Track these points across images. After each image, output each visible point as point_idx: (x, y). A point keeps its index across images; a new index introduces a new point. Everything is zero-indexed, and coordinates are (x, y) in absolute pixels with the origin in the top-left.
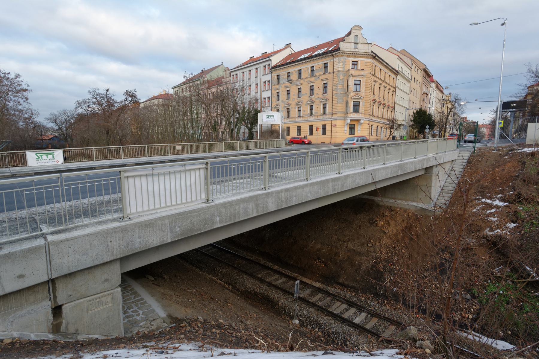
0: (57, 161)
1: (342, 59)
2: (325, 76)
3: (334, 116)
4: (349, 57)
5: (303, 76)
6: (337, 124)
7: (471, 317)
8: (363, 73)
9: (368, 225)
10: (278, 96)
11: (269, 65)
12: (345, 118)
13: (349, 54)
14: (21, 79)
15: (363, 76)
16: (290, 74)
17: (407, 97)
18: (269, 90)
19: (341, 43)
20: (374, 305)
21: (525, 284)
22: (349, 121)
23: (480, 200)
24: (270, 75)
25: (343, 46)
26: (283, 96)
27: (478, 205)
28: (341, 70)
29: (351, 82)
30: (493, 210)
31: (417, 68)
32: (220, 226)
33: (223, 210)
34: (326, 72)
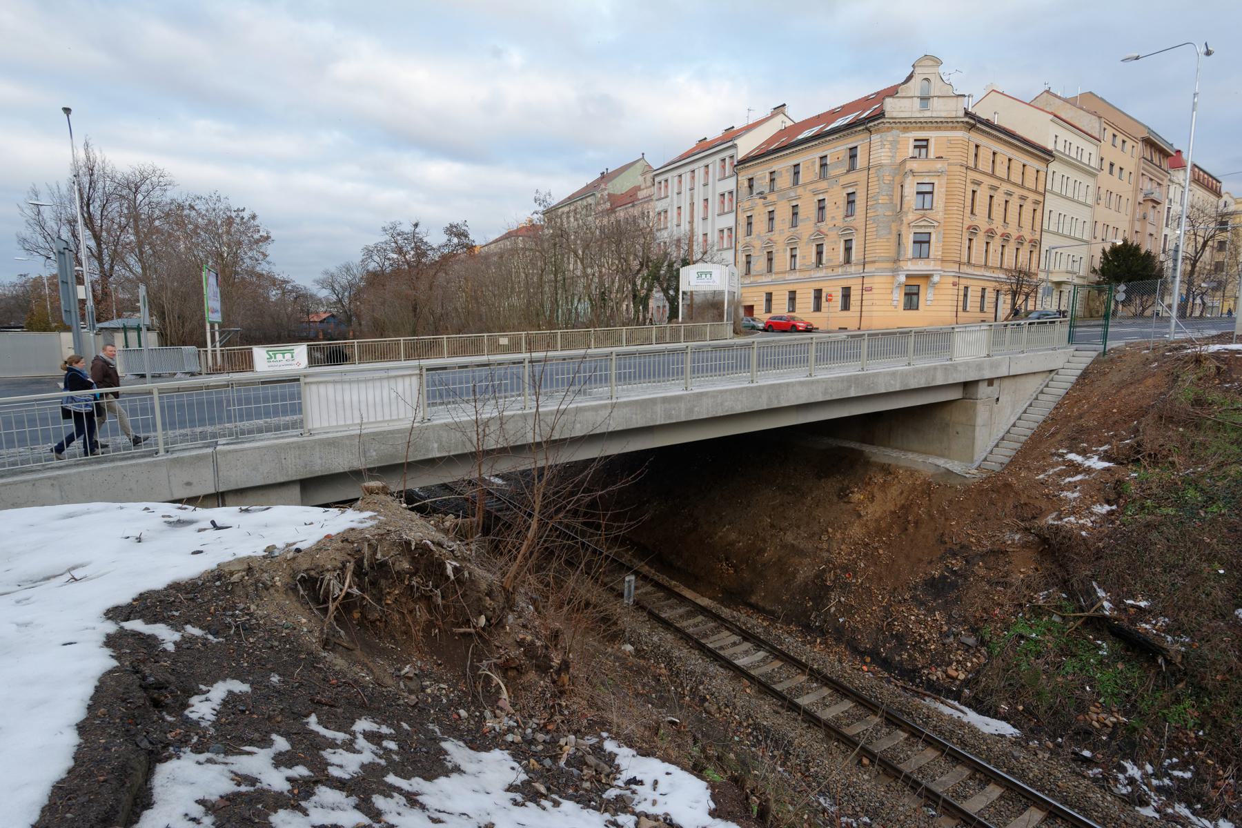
0: (298, 364)
2: (852, 177)
3: (868, 268)
4: (906, 130)
5: (802, 178)
6: (874, 286)
7: (962, 676)
8: (939, 165)
9: (835, 499)
10: (750, 224)
11: (732, 157)
13: (906, 124)
14: (256, 222)
15: (939, 174)
17: (1084, 214)
18: (731, 212)
19: (888, 101)
20: (791, 642)
21: (1079, 622)
22: (902, 279)
23: (1062, 456)
24: (734, 179)
25: (892, 107)
26: (760, 224)
27: (1058, 464)
28: (885, 161)
29: (910, 189)
30: (1079, 477)
31: (1120, 137)
32: (438, 455)
33: (445, 434)
34: (852, 168)
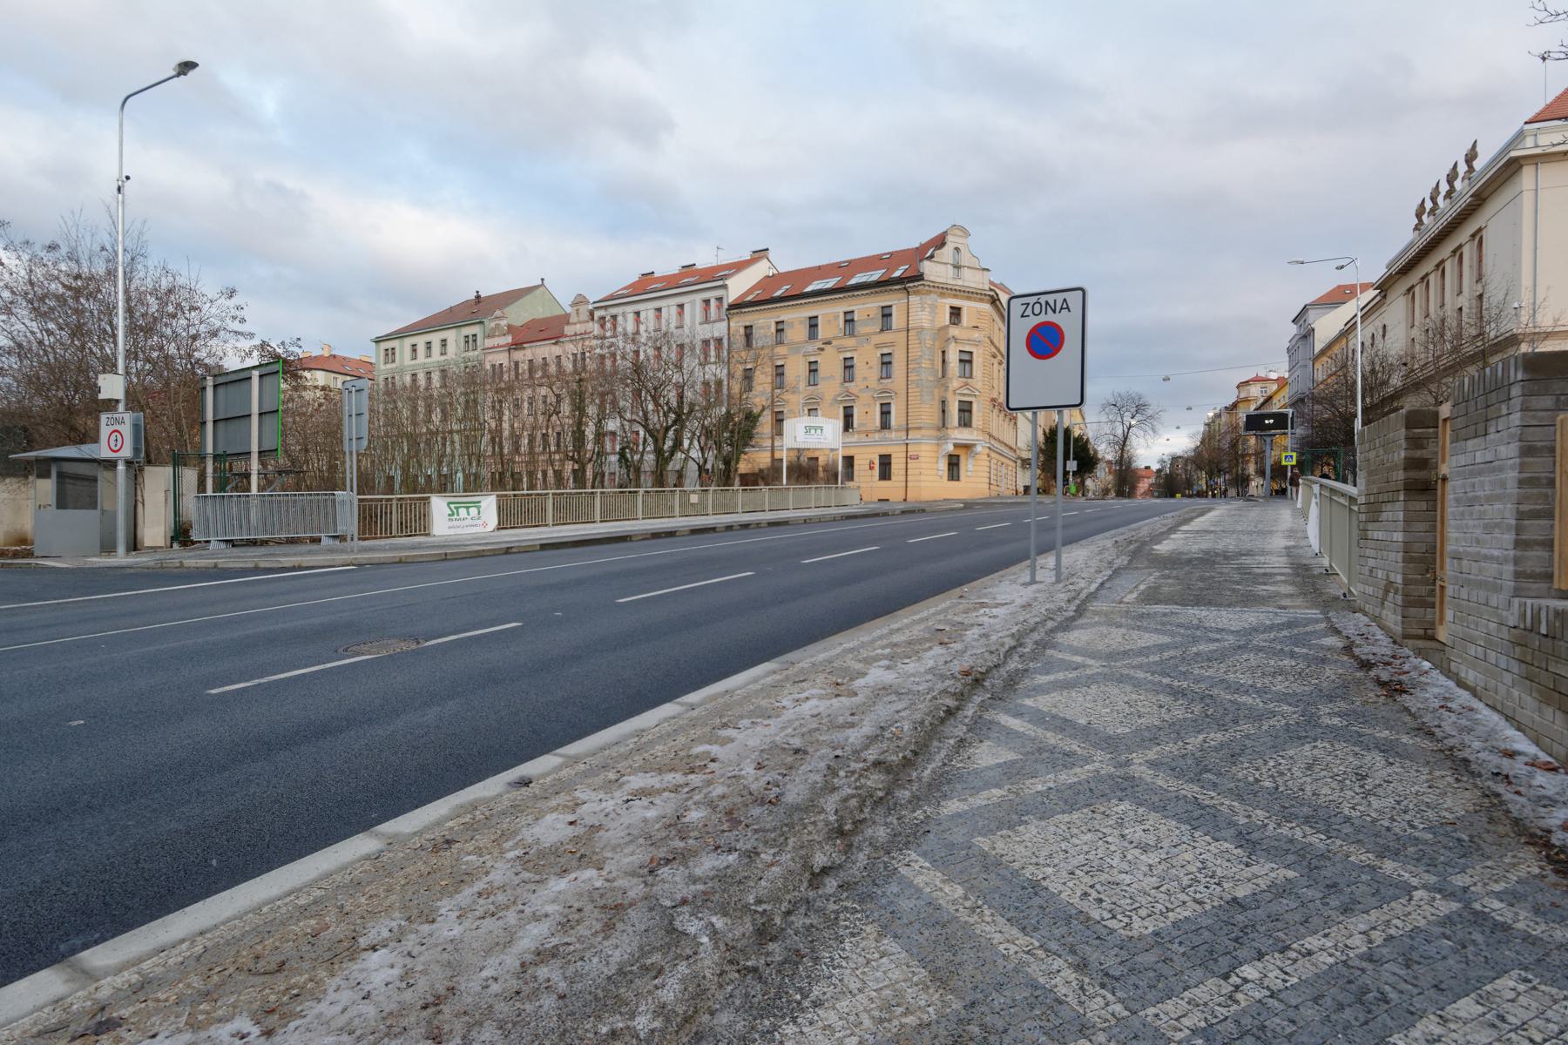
1: (930, 299)
2: (887, 337)
4: (942, 295)
8: (976, 335)
11: (720, 299)
12: (939, 439)
13: (944, 290)
15: (977, 343)
16: (785, 326)
28: (926, 325)
29: (953, 357)
34: (886, 327)
